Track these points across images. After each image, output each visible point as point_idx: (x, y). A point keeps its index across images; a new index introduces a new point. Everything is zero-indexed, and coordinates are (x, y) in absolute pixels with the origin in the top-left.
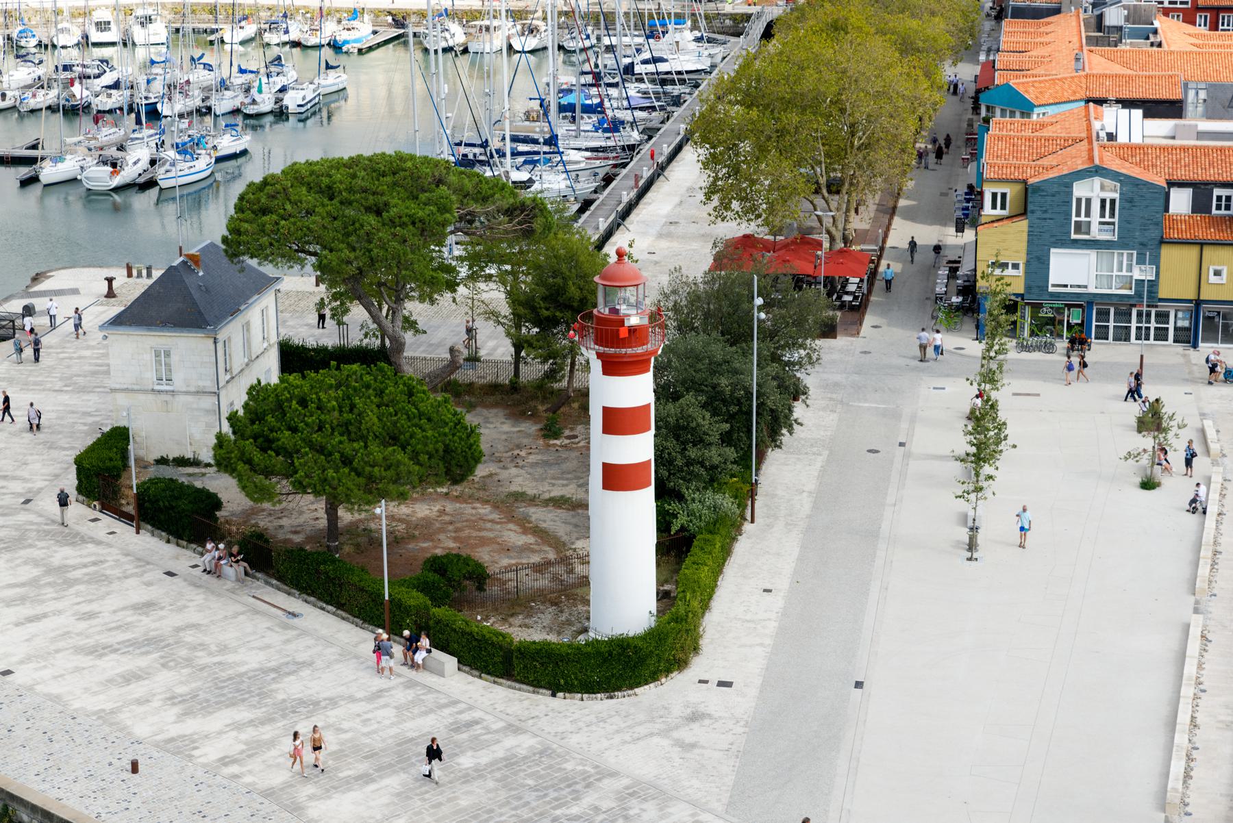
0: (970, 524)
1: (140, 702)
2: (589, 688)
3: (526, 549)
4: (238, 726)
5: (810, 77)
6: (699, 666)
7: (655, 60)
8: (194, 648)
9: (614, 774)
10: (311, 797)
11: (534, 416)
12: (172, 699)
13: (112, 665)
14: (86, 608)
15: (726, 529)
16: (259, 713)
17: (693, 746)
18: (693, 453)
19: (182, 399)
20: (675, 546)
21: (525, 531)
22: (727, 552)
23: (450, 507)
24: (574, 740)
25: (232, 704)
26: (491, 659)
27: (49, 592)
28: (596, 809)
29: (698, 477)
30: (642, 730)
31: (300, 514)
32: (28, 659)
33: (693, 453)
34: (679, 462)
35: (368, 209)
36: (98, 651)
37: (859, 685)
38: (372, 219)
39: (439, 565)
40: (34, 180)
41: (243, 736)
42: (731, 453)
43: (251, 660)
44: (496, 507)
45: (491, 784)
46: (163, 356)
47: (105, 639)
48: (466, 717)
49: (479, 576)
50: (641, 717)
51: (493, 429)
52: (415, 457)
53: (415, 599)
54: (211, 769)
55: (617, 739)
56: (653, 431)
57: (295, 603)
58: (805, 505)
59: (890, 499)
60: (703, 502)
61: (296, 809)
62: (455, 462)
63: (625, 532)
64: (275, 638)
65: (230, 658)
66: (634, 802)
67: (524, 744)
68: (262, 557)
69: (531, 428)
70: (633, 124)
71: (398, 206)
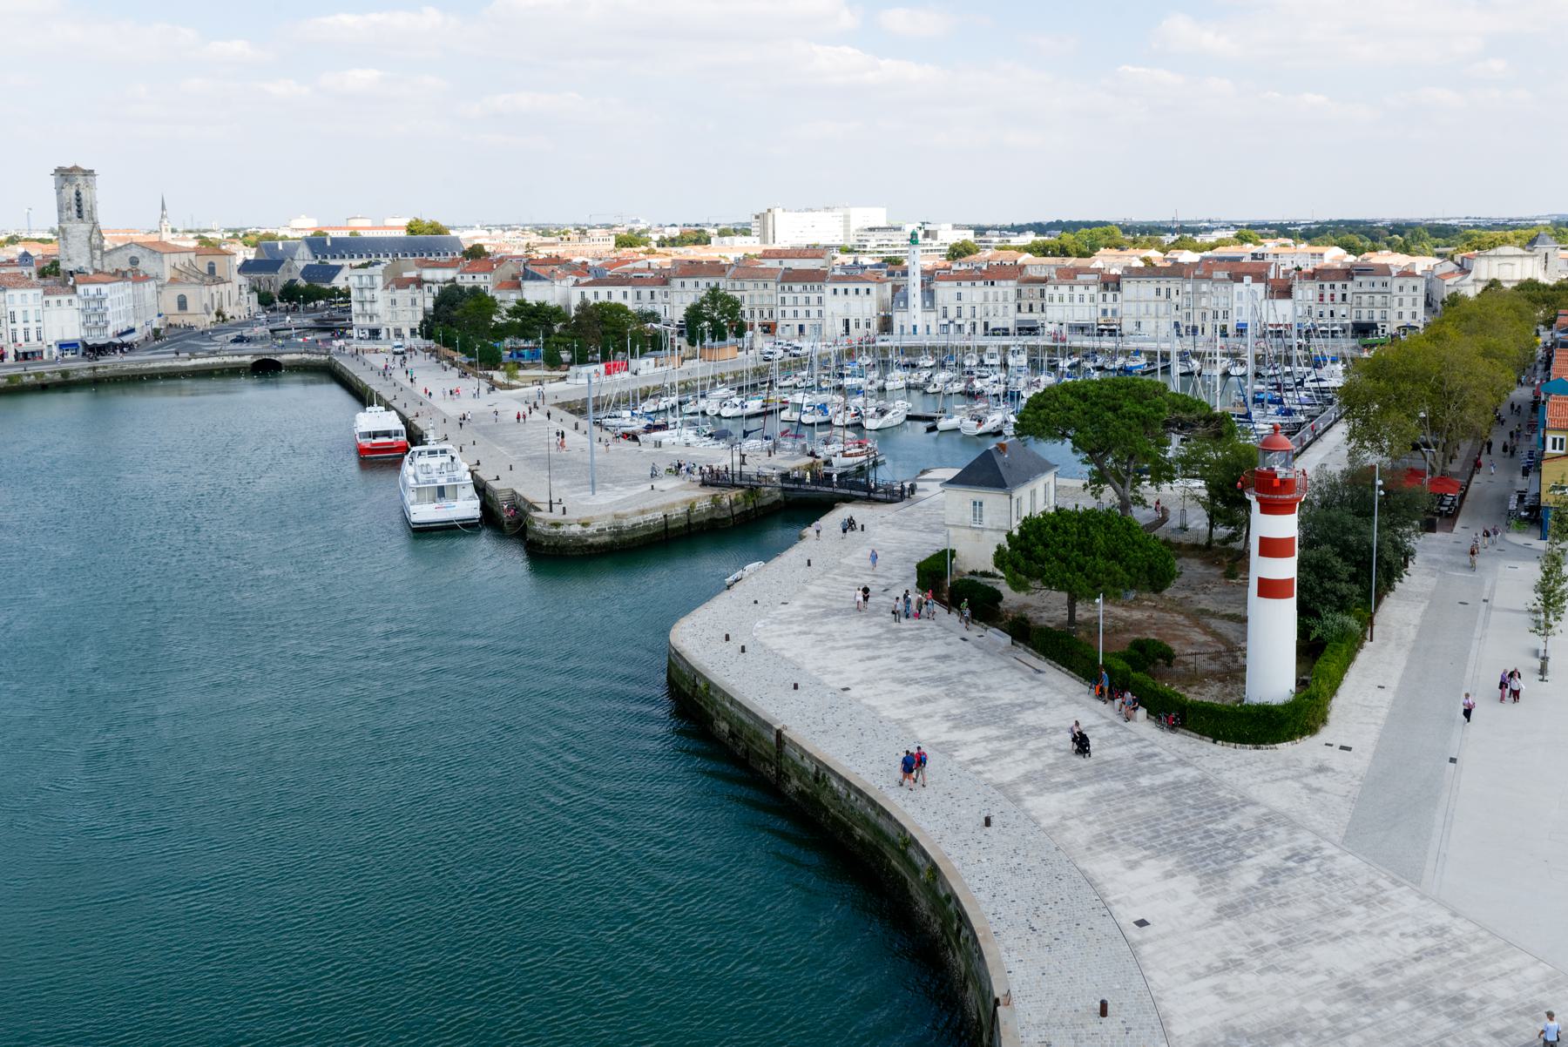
0: (1542, 654)
1: (926, 716)
2: (1241, 739)
3: (1205, 644)
4: (987, 739)
5: (1419, 360)
6: (1325, 734)
7: (1319, 380)
8: (969, 686)
9: (1255, 804)
10: (1028, 794)
11: (1220, 564)
12: (948, 717)
13: (914, 691)
14: (906, 655)
15: (1353, 642)
16: (1004, 732)
17: (1318, 790)
18: (1328, 585)
19: (987, 533)
20: (1310, 649)
21: (1206, 633)
22: (1351, 658)
23: (1156, 614)
24: (1226, 776)
25: (987, 724)
26: (1176, 715)
27: (886, 643)
28: (1239, 828)
29: (1331, 602)
30: (1279, 774)
31: (1047, 605)
32: (862, 682)
33: (1328, 585)
34: (1318, 590)
35: (1109, 409)
36: (906, 682)
37: (1453, 760)
38: (1110, 414)
39: (1140, 646)
40: (934, 429)
41: (990, 747)
42: (1356, 589)
43: (1005, 697)
44: (1187, 616)
45: (1161, 800)
46: (978, 505)
47: (914, 675)
48: (1149, 751)
49: (1168, 656)
50: (1280, 765)
51: (1192, 568)
52: (1128, 569)
53: (1121, 665)
54: (963, 766)
55: (1260, 778)
56: (1296, 557)
57: (1042, 664)
58: (1411, 634)
59: (1477, 635)
60: (1335, 620)
61: (1017, 800)
62: (1156, 578)
63: (1274, 632)
64: (1024, 685)
65: (992, 695)
66: (1269, 826)
67: (1189, 774)
68: (1023, 632)
69: (1219, 572)
70: (1301, 412)
71: (1128, 406)
